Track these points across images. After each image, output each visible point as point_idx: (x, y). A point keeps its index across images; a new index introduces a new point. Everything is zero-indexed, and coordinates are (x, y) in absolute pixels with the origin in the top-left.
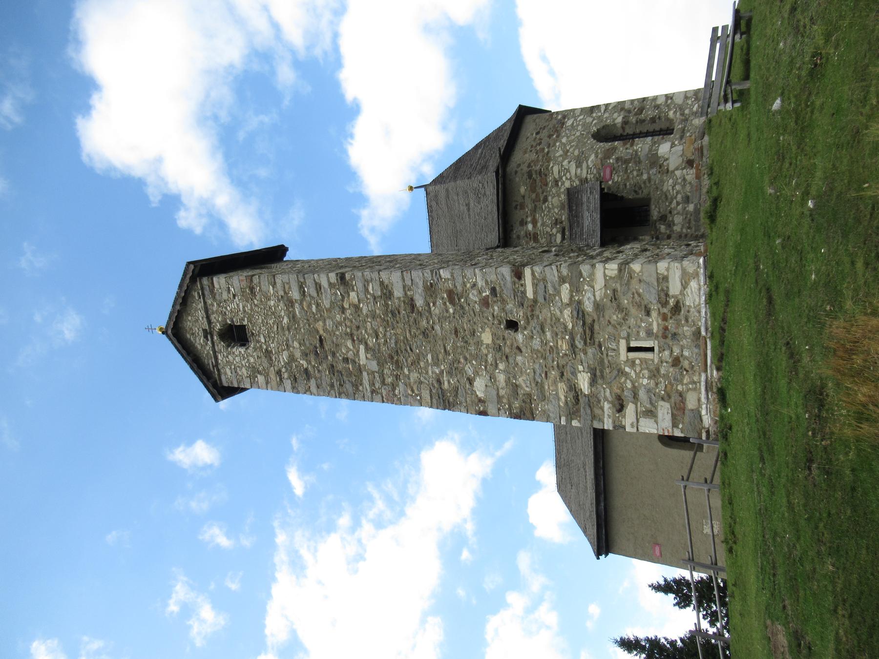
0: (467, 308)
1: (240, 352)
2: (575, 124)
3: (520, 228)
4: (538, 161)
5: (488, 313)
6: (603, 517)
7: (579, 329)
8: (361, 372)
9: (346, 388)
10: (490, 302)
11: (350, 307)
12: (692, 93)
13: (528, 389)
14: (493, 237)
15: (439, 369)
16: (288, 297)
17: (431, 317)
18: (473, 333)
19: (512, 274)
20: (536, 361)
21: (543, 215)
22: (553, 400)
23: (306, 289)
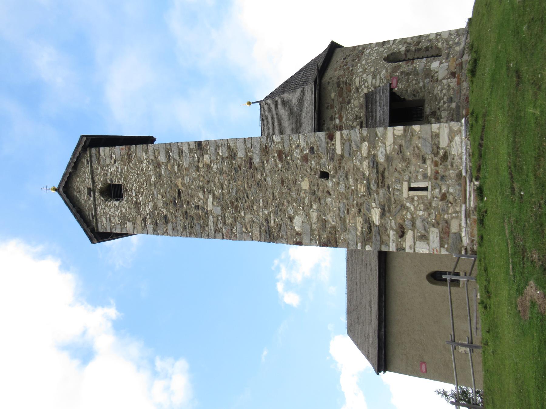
0: (292, 164)
1: (115, 204)
2: (371, 53)
3: (330, 122)
4: (344, 75)
5: (307, 167)
6: (383, 340)
7: (374, 176)
8: (208, 216)
9: (195, 229)
10: (309, 158)
11: (203, 166)
12: (454, 32)
13: (334, 223)
15: (268, 211)
16: (157, 160)
17: (265, 171)
18: (295, 182)
19: (326, 136)
20: (341, 201)
21: (347, 112)
22: (352, 231)
23: (171, 154)
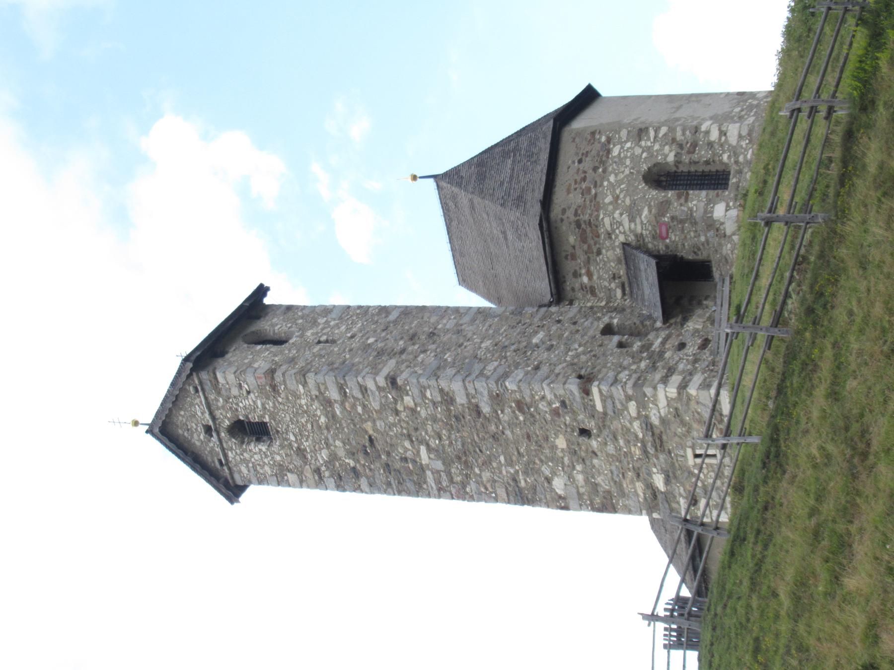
2: (622, 155)
3: (574, 280)
7: (649, 438)
8: (424, 471)
13: (607, 487)
14: (543, 287)
16: (324, 398)
17: (500, 423)
18: (547, 439)
23: (347, 391)
